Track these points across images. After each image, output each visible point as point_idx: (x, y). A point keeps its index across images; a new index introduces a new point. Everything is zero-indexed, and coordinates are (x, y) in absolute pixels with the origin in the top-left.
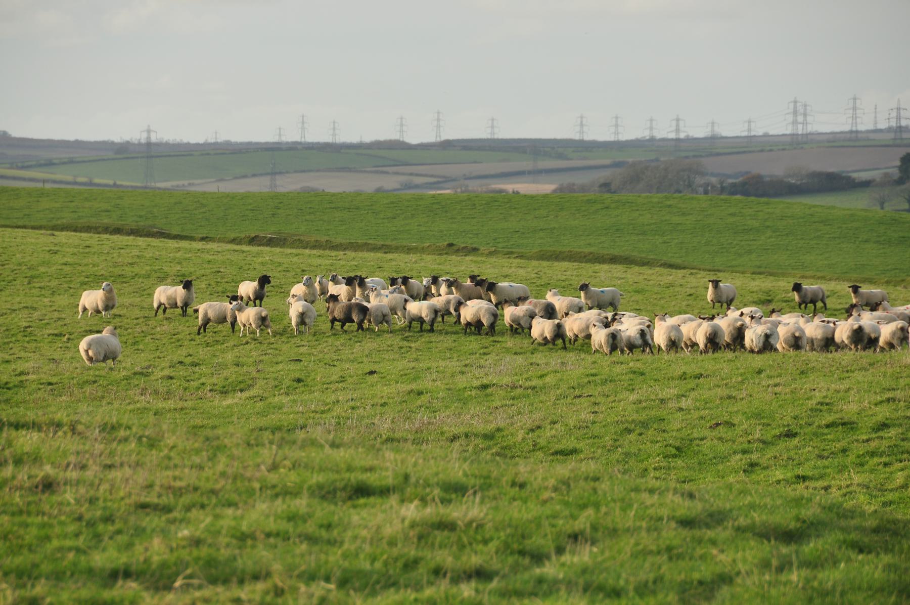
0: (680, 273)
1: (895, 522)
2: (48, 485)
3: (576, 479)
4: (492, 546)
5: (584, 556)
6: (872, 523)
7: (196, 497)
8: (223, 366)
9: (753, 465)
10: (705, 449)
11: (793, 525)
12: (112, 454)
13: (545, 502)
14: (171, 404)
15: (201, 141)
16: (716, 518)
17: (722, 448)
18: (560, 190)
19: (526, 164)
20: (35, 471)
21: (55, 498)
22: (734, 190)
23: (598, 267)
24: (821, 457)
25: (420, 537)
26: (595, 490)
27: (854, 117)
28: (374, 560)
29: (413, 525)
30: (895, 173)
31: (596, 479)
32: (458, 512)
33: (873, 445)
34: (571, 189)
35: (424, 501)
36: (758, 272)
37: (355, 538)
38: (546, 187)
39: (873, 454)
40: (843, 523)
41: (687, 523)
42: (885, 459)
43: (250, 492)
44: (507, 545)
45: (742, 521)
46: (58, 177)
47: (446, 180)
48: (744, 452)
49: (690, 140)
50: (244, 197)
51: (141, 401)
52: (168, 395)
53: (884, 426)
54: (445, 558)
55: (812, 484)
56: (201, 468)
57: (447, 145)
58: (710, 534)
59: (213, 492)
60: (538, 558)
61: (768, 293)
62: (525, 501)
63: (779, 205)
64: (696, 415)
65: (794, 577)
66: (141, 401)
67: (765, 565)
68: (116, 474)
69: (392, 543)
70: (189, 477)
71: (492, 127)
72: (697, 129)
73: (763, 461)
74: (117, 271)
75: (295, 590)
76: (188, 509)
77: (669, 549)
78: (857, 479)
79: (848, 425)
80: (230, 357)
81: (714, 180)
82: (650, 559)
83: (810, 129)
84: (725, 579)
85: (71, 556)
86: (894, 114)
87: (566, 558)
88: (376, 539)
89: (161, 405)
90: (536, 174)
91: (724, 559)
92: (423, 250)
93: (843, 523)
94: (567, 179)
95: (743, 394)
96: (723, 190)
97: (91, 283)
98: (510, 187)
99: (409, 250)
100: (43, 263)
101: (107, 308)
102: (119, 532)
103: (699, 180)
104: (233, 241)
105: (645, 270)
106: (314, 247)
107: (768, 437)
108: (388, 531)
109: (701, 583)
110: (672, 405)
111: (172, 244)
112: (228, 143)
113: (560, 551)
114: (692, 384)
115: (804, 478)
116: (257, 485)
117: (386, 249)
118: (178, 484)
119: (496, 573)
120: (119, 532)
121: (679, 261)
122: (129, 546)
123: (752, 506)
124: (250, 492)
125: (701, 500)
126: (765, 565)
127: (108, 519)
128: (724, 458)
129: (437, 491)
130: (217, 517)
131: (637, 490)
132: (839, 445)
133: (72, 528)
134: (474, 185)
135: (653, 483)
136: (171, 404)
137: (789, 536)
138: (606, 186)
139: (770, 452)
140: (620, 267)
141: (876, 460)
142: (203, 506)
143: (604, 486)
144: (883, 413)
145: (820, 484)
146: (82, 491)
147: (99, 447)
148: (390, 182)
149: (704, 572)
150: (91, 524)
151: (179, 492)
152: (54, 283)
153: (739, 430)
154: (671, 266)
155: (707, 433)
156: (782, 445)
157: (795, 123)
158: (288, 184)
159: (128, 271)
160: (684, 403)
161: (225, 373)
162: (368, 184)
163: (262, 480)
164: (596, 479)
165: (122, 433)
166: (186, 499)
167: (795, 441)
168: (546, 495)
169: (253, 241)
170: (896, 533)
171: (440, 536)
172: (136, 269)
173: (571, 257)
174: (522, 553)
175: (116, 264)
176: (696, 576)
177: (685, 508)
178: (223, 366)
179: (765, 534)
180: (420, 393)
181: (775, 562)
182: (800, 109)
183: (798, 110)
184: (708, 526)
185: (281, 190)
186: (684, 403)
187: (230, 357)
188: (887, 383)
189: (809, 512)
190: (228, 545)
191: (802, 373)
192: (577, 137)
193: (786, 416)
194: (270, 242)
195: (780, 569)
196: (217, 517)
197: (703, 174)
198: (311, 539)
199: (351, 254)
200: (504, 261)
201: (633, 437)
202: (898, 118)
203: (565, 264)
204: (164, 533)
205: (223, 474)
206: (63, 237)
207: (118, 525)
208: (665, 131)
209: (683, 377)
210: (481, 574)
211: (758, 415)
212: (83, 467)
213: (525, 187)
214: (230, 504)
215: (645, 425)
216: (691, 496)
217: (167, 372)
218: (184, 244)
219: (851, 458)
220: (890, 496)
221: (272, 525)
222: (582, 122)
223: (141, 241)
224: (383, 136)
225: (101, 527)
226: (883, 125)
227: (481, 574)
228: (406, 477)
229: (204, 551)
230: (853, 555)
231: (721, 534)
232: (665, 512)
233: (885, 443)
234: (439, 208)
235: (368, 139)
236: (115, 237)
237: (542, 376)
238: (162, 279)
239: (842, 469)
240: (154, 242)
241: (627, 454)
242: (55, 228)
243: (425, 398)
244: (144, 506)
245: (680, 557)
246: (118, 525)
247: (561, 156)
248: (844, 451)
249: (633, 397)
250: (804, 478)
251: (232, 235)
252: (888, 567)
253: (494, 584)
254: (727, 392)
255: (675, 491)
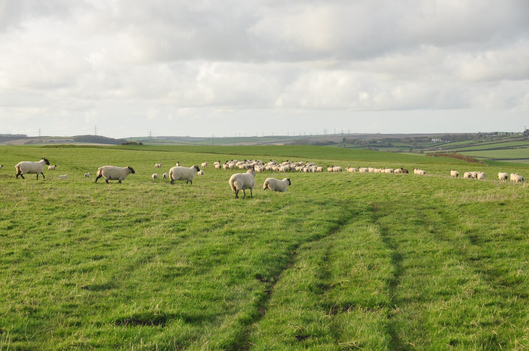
0: (305, 159)
1: (341, 201)
2: (195, 197)
3: (287, 194)
4: (272, 206)
5: (288, 208)
6: (338, 201)
7: (220, 198)
8: (226, 176)
9: (318, 192)
10: (310, 189)
11: (324, 202)
12: (206, 191)
13: (281, 199)
14: (217, 182)
15: (222, 137)
16: (311, 201)
17: (313, 189)
18: (285, 144)
19: (279, 140)
20: (193, 194)
21: (197, 199)
22: (315, 144)
23: (291, 158)
24: (329, 190)
25: (259, 205)
26: (290, 196)
27: (335, 132)
28: (251, 209)
29: (258, 203)
30: (342, 141)
31: (290, 194)
32: (265, 201)
33: (339, 188)
34: (286, 144)
35: (260, 199)
36: (319, 158)
37: (248, 205)
38: (282, 144)
39: (338, 189)
40: (333, 201)
41: (306, 202)
42: (340, 190)
43: (230, 198)
44: (274, 206)
45: (315, 201)
46: (198, 144)
47: (265, 143)
48: (316, 189)
49: (306, 136)
50: (230, 147)
51: (212, 182)
52: (217, 181)
53: (340, 185)
54: (264, 208)
55: (328, 195)
56: (221, 193)
57: (265, 137)
58: (309, 204)
59: (224, 197)
60: (280, 208)
61: (320, 162)
62: (278, 198)
63: (322, 147)
64: (308, 183)
65: (324, 211)
66: (212, 182)
67: (319, 209)
68: (207, 195)
69: (254, 206)
70: (219, 195)
71: (40, 132)
72: (308, 134)
73: (320, 191)
74: (208, 160)
75: (238, 214)
76: (219, 200)
77: (303, 206)
78: (335, 194)
79: (334, 185)
80: (227, 174)
81: (311, 143)
82: (299, 208)
83: (327, 134)
84: (312, 211)
85: (199, 208)
86: (342, 131)
87: (285, 208)
88: (252, 205)
89: (215, 183)
90: (281, 142)
91: (312, 208)
92: (261, 155)
93: (333, 201)
94: (286, 143)
95: (316, 179)
96: (313, 144)
97: (204, 162)
98: (276, 144)
99: (258, 155)
100: (195, 158)
101: (206, 166)
102: (207, 204)
103: (308, 143)
104: (228, 154)
105: (299, 158)
106: (242, 155)
107: (320, 187)
108: (254, 204)
109: (308, 212)
110: (304, 181)
111: (217, 155)
112: (227, 137)
113: (284, 207)
114: (307, 178)
115: (327, 194)
116: (231, 196)
117: (254, 155)
118: (217, 196)
119: (273, 211)
120: (207, 204)
121: (305, 157)
122: (209, 207)
123: (317, 199)
124: (230, 198)
125: (308, 198)
126: (319, 209)
127: (205, 202)
128: (313, 191)
129: (262, 197)
130: (224, 202)
131: (297, 196)
132: (333, 188)
133: (199, 204)
134: (269, 144)
135: (300, 195)
136: (217, 182)
137: (323, 204)
138: (292, 144)
139: (321, 189)
140: (295, 158)
141: (339, 190)
142: (221, 200)
143: (292, 196)
144: (340, 182)
145: (329, 195)
146: (201, 197)
147: (204, 190)
148: (255, 144)
149: (309, 210)
150: (202, 203)
151: (217, 198)
152: (197, 162)
153: (315, 186)
154: (304, 158)
155: (310, 186)
156: (323, 188)
157: (325, 133)
158: (237, 144)
159: (210, 160)
160: (306, 181)
161: (226, 177)
162: (251, 144)
163: (232, 195)
164: (290, 194)
165: (208, 187)
166: (218, 199)
167: (325, 187)
168: (281, 197)
169: (231, 154)
170: (341, 203)
171: (263, 205)
172: (211, 159)
173: (286, 156)
174: (277, 207)
175: (208, 159)
176: (307, 211)
177: (305, 199)
178: (226, 176)
179: (319, 204)
180: (260, 180)
181: (321, 208)
182: (326, 130)
183: (325, 131)
184: (309, 202)
185: (236, 145)
186: (306, 181)
187: (227, 174)
188: (341, 177)
189: (327, 200)
190: (226, 207)
191: (326, 176)
192: (287, 135)
193: (323, 183)
194: (234, 154)
195: (322, 209)
196: (224, 202)
197: (309, 142)
198: (240, 206)
199: (248, 156)
200: (275, 157)
201: (297, 187)
202: (342, 132)
203: (285, 157)
204: (215, 205)
205: (225, 194)
206: (198, 154)
207: (207, 203)
208: (302, 134)
209: (306, 177)
210: (270, 211)
211: (319, 183)
212: (201, 193)
213: (278, 144)
214: (227, 200)
215: (299, 185)
216: (307, 197)
217: (216, 177)
218: (219, 155)
219: (335, 190)
220: (341, 197)
221: (233, 203)
222: (40, 131)
223: (212, 154)
224: (254, 136)
225: (204, 204)
226: (340, 133)
227: (270, 211)
228: (257, 195)
229: (222, 208)
230: (334, 206)
231: (311, 204)
232: (302, 200)
233: (340, 188)
234: (263, 148)
235: (251, 136)
236: (208, 154)
237: (281, 177)
238: (215, 161)
239: (333, 192)
240: (214, 154)
241: (296, 190)
242: (197, 152)
243: (261, 181)
244: (211, 200)
245: (304, 208)
246: (207, 203)
247: (285, 139)
248: (333, 189)
249: (297, 180)
250: (327, 194)
251: (228, 153)
252: (340, 209)
253: (272, 213)
254: (313, 179)
255: (304, 196)
